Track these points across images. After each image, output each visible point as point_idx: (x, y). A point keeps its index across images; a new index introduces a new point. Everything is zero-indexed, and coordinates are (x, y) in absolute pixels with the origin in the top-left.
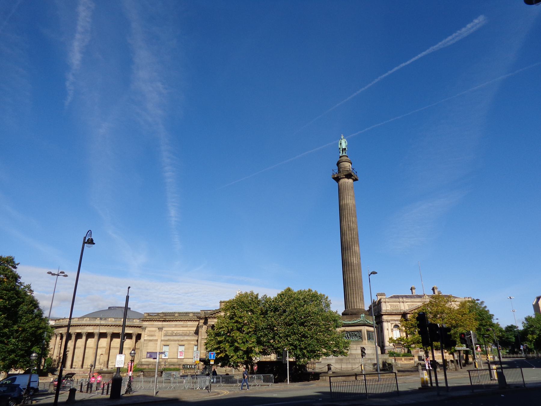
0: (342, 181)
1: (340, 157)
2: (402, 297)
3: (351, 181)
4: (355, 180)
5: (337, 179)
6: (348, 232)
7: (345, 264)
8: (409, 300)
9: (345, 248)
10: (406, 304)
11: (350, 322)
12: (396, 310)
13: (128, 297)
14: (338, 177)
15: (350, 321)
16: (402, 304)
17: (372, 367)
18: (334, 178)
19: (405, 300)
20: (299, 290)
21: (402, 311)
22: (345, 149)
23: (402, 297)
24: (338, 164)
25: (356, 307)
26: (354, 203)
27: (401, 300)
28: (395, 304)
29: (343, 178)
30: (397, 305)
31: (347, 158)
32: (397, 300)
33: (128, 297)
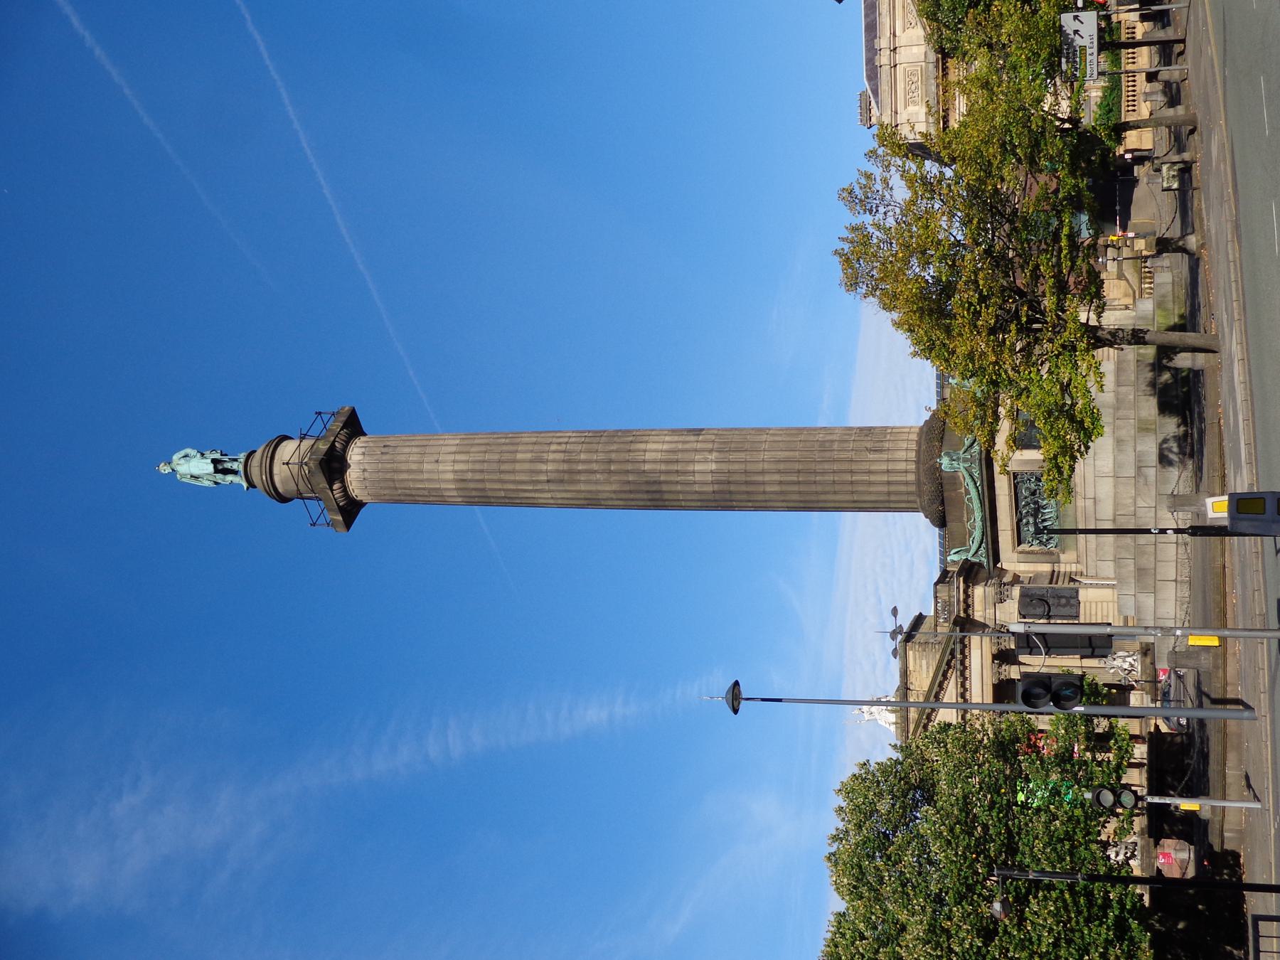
0: (356, 491)
1: (251, 485)
2: (872, 51)
3: (355, 453)
4: (353, 427)
5: (350, 509)
6: (583, 487)
7: (727, 497)
8: (885, 21)
9: (654, 495)
10: (902, 38)
11: (978, 515)
12: (925, 82)
13: (780, 700)
14: (342, 510)
15: (971, 512)
16: (902, 56)
17: (1174, 473)
18: (348, 523)
19: (883, 42)
20: (826, 875)
21: (932, 57)
22: (215, 461)
23: (872, 51)
24: (283, 499)
25: (911, 477)
26: (452, 442)
27: (884, 59)
28: (900, 86)
29: (344, 489)
30: (908, 74)
31: (258, 455)
32: (884, 73)
33: (780, 700)
